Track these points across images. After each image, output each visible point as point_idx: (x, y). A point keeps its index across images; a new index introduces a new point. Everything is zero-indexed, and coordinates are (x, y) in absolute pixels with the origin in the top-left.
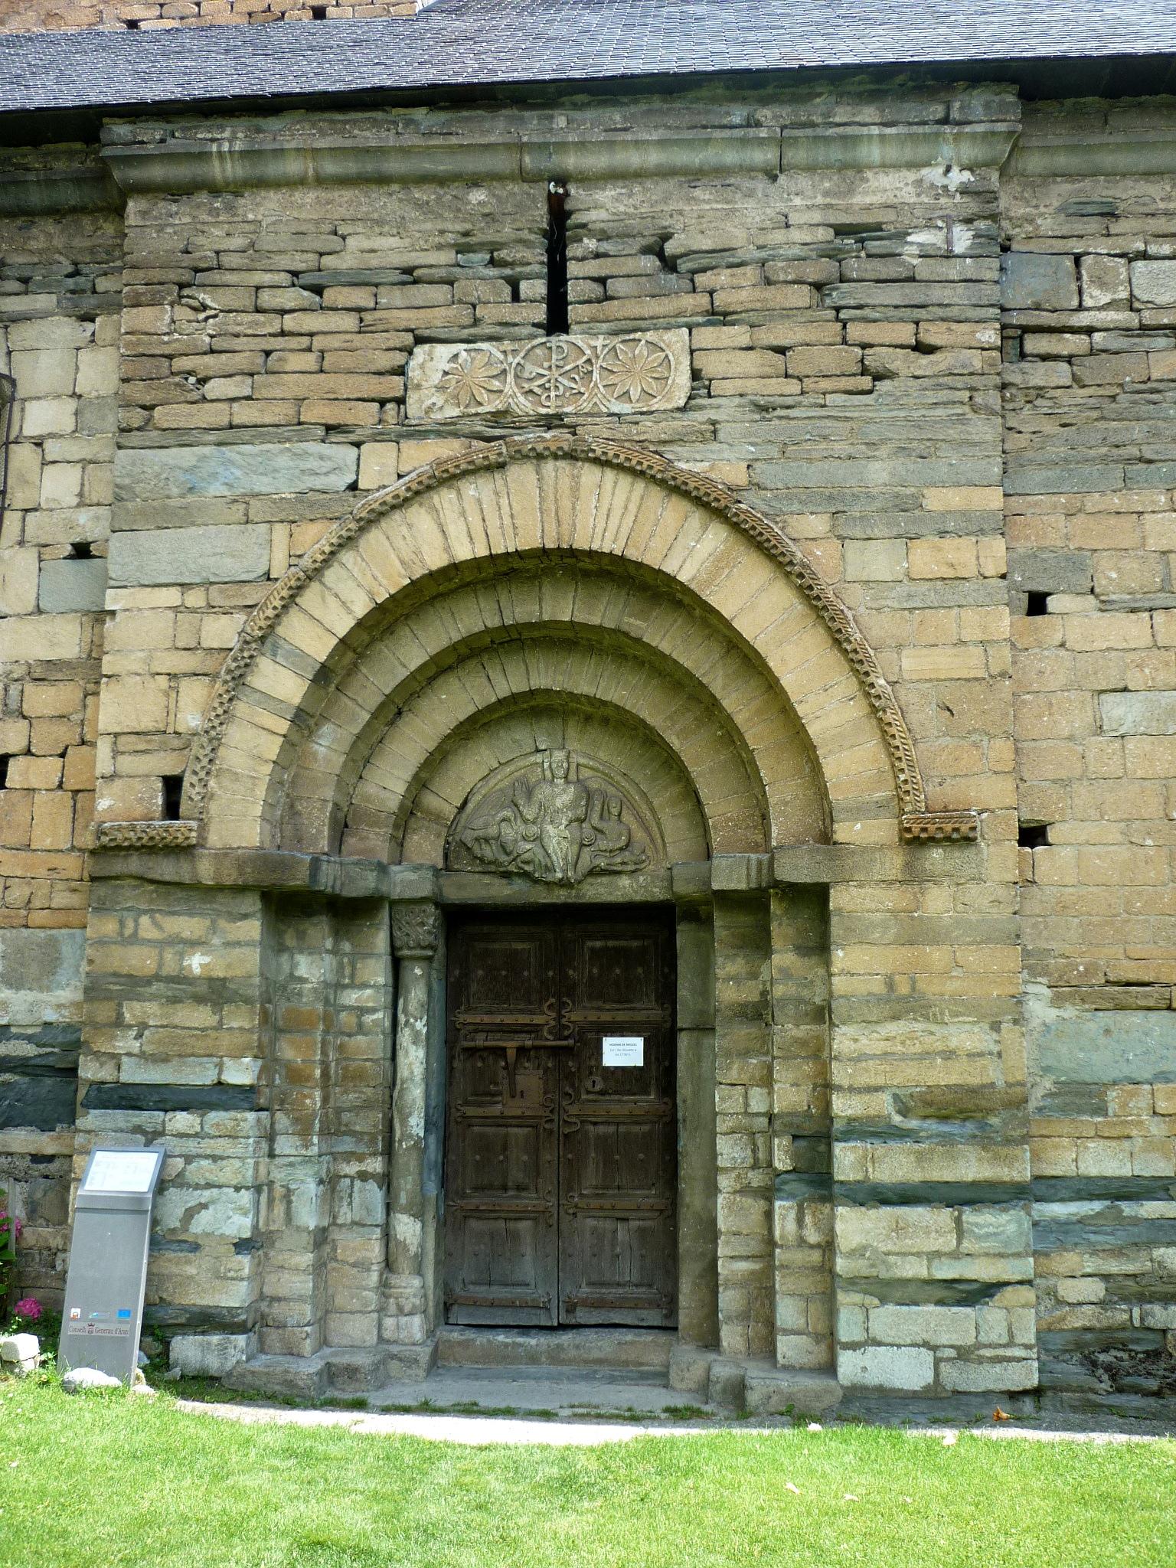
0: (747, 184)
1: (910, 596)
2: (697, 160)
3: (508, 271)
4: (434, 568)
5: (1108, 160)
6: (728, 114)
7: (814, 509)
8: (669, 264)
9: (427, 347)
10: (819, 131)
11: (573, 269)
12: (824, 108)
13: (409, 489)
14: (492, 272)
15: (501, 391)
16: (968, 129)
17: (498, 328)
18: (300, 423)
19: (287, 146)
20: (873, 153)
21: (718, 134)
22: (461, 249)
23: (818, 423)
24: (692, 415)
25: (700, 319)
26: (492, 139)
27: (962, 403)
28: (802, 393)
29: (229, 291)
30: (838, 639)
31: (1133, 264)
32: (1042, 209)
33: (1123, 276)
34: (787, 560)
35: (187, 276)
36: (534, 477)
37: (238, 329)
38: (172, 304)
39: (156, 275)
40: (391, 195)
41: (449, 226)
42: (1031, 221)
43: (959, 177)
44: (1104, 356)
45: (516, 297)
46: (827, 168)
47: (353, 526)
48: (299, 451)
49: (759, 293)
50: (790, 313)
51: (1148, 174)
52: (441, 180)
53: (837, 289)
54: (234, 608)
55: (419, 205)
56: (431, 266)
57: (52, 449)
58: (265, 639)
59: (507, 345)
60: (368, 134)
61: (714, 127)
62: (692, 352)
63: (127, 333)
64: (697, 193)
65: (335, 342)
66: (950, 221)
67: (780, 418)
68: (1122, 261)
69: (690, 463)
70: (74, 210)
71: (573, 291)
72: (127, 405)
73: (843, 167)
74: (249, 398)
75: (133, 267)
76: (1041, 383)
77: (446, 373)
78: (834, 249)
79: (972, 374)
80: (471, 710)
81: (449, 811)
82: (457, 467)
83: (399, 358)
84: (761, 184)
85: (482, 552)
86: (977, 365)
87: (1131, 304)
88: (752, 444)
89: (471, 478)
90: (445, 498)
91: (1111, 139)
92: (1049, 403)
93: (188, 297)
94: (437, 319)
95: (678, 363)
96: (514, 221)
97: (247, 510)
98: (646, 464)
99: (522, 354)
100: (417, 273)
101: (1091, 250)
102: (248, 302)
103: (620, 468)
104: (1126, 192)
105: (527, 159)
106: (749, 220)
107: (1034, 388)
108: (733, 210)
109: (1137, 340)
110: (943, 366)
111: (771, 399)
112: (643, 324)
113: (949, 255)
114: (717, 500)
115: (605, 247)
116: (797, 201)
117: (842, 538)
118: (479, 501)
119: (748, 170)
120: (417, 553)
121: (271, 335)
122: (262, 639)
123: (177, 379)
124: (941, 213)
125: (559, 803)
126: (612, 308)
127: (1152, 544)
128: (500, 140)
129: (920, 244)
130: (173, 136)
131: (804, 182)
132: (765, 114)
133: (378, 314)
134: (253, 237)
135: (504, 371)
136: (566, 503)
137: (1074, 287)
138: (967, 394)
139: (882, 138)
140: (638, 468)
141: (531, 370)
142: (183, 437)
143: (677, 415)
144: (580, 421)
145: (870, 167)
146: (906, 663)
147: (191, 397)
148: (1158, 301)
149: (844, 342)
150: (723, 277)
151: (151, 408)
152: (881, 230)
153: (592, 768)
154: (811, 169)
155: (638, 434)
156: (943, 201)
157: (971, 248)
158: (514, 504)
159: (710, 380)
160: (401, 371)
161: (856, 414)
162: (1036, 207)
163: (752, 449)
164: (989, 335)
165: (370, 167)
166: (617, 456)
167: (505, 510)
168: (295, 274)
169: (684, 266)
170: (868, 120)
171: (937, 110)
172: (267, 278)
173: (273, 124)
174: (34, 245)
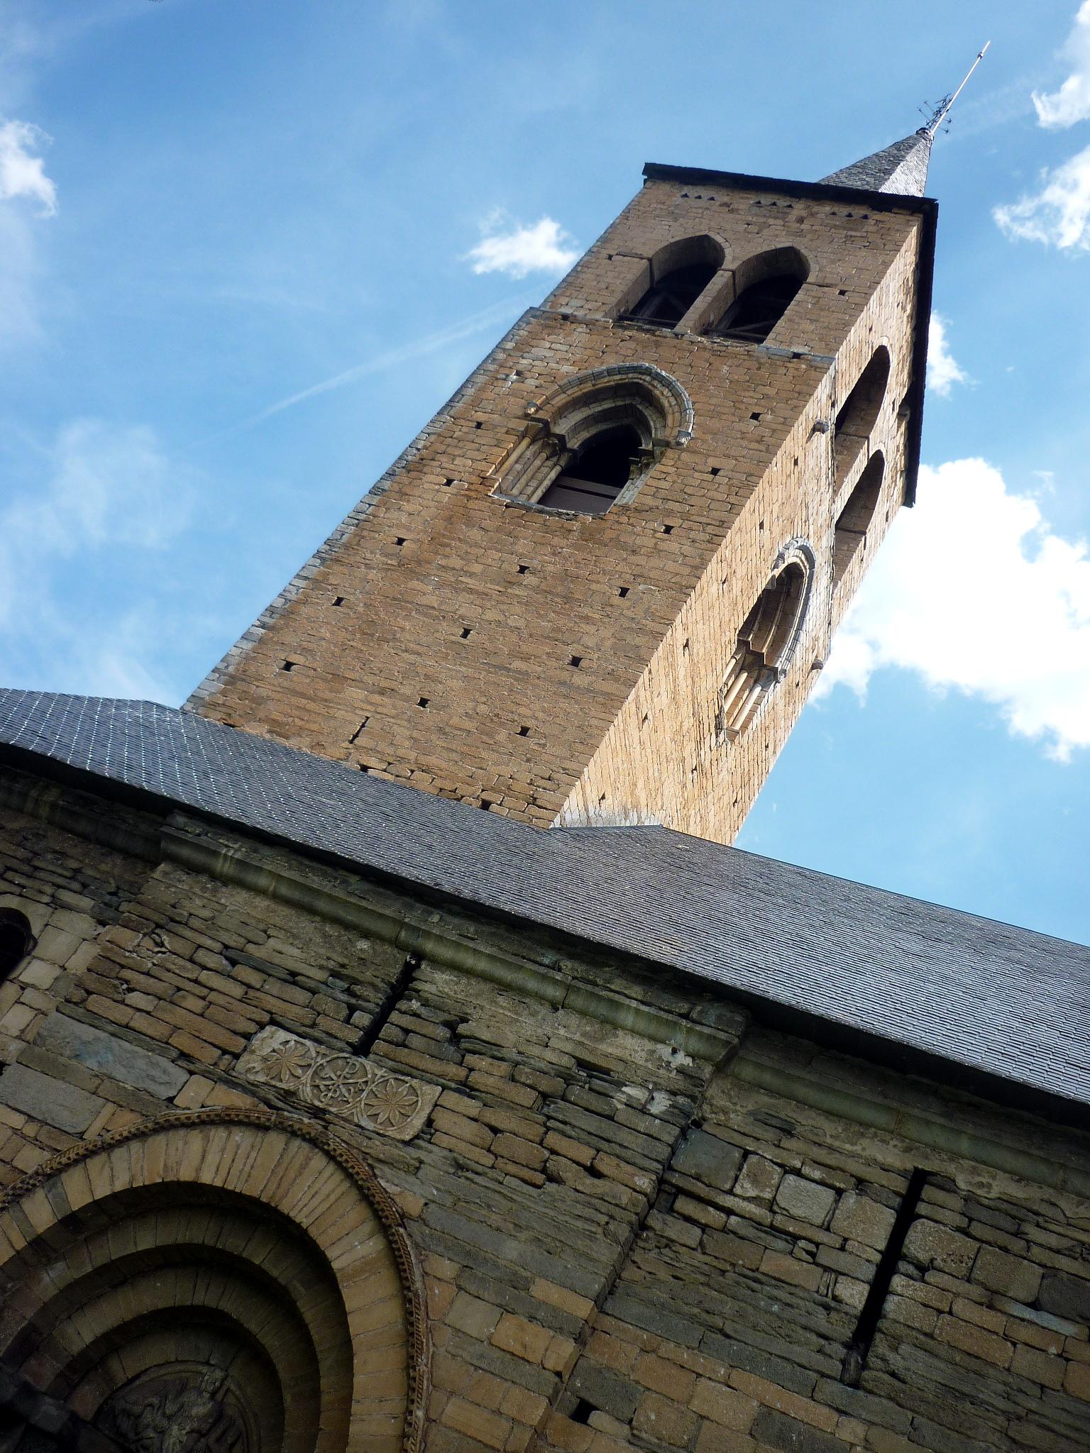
0: (535, 1006)
1: (482, 1356)
2: (509, 978)
3: (353, 1001)
4: (182, 1179)
5: (802, 1091)
6: (543, 955)
7: (451, 1256)
8: (456, 1038)
9: (274, 1028)
10: (596, 990)
11: (394, 1017)
12: (608, 975)
13: (199, 1117)
14: (344, 997)
15: (299, 1078)
16: (698, 1028)
17: (324, 1035)
18: (167, 1043)
19: (265, 867)
20: (629, 1019)
21: (529, 966)
22: (334, 974)
23: (490, 1194)
24: (410, 1150)
25: (453, 1085)
26: (387, 912)
27: (599, 1224)
28: (493, 1167)
29: (182, 941)
30: (410, 1364)
31: (787, 1175)
32: (738, 1108)
33: (775, 1182)
34: (408, 1284)
35: (163, 921)
36: (282, 1146)
37: (172, 967)
38: (145, 935)
39: (147, 912)
40: (313, 922)
41: (335, 956)
42: (725, 1113)
43: (682, 1059)
44: (731, 1235)
45: (347, 1020)
46: (594, 1018)
47: (150, 1125)
48: (154, 1061)
49: (501, 1084)
50: (516, 1107)
51: (829, 1114)
52: (348, 926)
53: (556, 1103)
54: (48, 1147)
55: (326, 936)
56: (309, 977)
57: (29, 996)
58: (50, 1176)
59: (323, 1049)
60: (315, 878)
61: (529, 960)
62: (436, 1105)
63: (108, 941)
64: (500, 999)
65: (221, 1000)
66: (657, 1087)
67: (467, 1179)
68: (779, 1170)
69: (389, 1183)
70: (136, 856)
71: (387, 1031)
72: (78, 985)
73: (604, 1021)
74: (148, 1013)
75: (138, 903)
76: (674, 1237)
77: (274, 1051)
78: (569, 1074)
79: (616, 1205)
80: (171, 1304)
81: (121, 1378)
82: (238, 1115)
83: (252, 1027)
84: (544, 1011)
85: (218, 1183)
86: (624, 1200)
87: (771, 1205)
88: (437, 1189)
89: (243, 1129)
90: (218, 1134)
91: (808, 1076)
92: (672, 1255)
93: (157, 934)
94: (293, 1013)
95: (422, 1109)
96: (376, 970)
97: (99, 1084)
98: (357, 1169)
99: (328, 1059)
100: (298, 978)
101: (760, 1152)
102: (188, 953)
103: (339, 1165)
104: (806, 1120)
105: (403, 934)
106: (523, 1031)
107: (666, 1238)
108: (518, 1021)
109: (763, 1235)
110: (599, 1191)
111: (469, 1162)
112: (415, 1072)
113: (643, 1111)
114: (387, 1217)
115: (424, 1012)
116: (562, 1032)
117: (460, 1288)
118: (238, 1147)
119: (540, 998)
120: (179, 1163)
121: (188, 979)
122: (49, 1176)
123: (117, 982)
124: (655, 1079)
125: (194, 1411)
126: (403, 1053)
127: (696, 1405)
128: (391, 915)
129: (629, 1095)
130: (206, 835)
131: (574, 1020)
132: (567, 964)
133: (258, 994)
134: (216, 913)
135: (309, 1066)
136: (292, 1174)
137: (732, 1174)
138: (606, 1219)
139: (637, 1010)
140: (350, 1170)
141: (328, 1072)
142: (95, 1020)
143: (400, 1145)
144: (336, 1120)
145: (623, 1028)
146: (449, 1409)
147: (117, 997)
148: (791, 1212)
149: (541, 1144)
150: (483, 1063)
151: (89, 993)
152: (609, 1075)
153: (236, 1397)
154: (583, 1013)
155: (366, 1147)
156: (662, 1071)
157: (663, 1113)
158: (258, 1159)
159: (437, 1130)
160: (248, 1036)
161: (519, 1199)
162: (735, 1104)
163: (435, 1193)
164: (644, 1182)
165: (307, 899)
166: (341, 1155)
167: (250, 1161)
168: (226, 947)
169: (465, 1045)
170: (634, 995)
171: (684, 1007)
172: (208, 942)
173: (266, 851)
174: (103, 867)
